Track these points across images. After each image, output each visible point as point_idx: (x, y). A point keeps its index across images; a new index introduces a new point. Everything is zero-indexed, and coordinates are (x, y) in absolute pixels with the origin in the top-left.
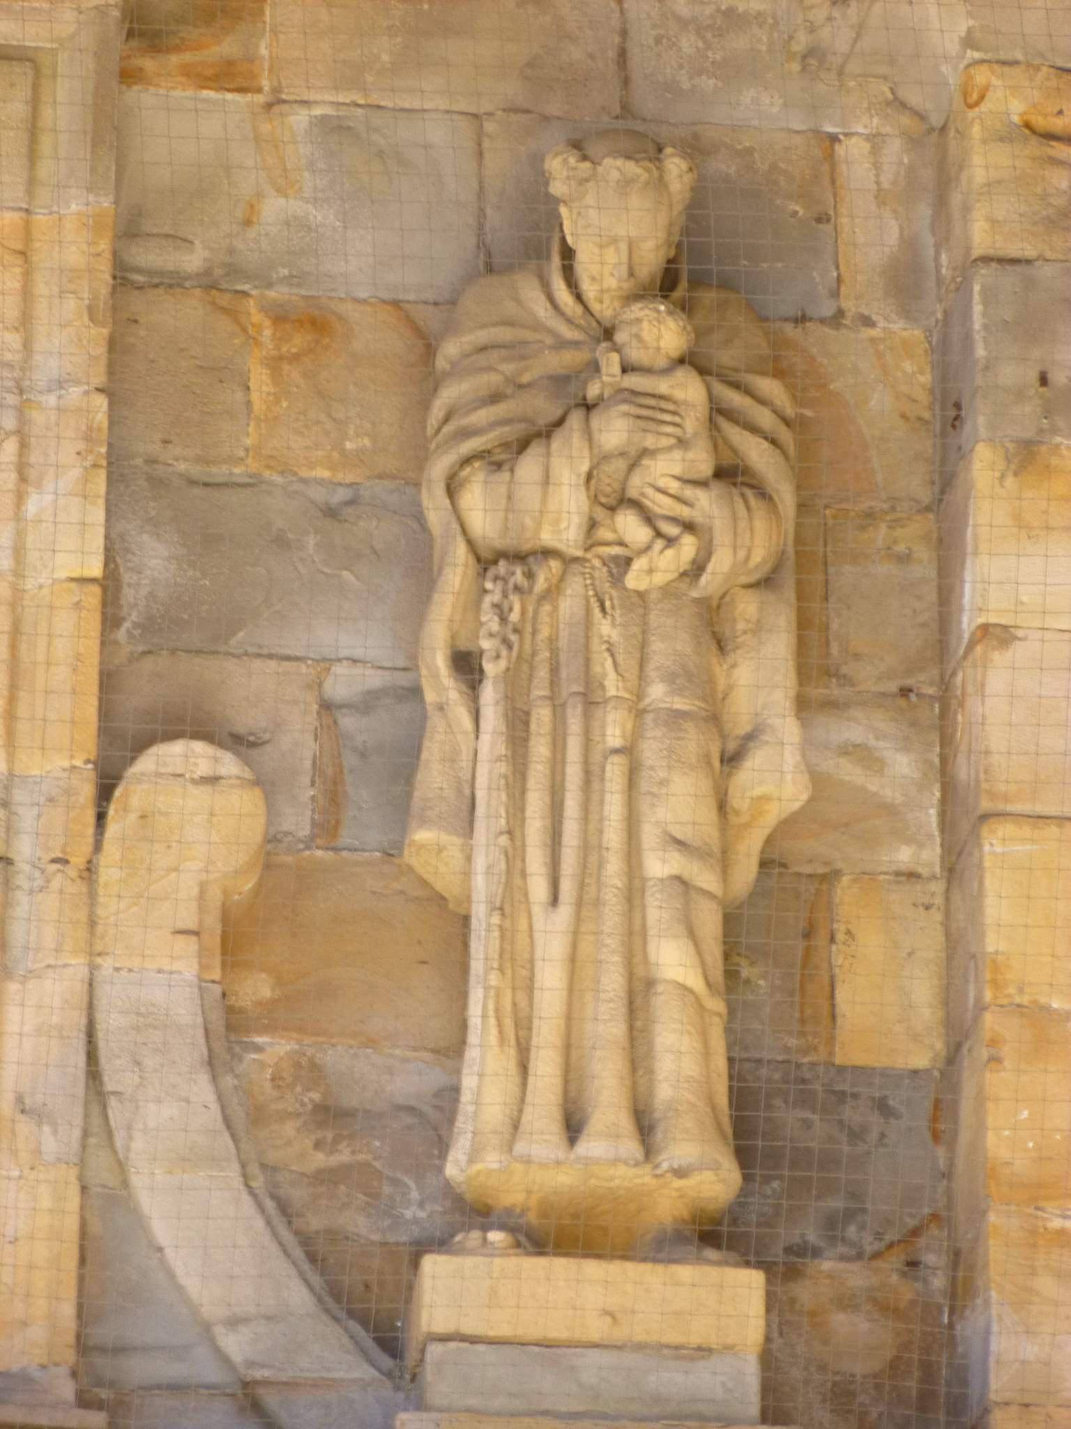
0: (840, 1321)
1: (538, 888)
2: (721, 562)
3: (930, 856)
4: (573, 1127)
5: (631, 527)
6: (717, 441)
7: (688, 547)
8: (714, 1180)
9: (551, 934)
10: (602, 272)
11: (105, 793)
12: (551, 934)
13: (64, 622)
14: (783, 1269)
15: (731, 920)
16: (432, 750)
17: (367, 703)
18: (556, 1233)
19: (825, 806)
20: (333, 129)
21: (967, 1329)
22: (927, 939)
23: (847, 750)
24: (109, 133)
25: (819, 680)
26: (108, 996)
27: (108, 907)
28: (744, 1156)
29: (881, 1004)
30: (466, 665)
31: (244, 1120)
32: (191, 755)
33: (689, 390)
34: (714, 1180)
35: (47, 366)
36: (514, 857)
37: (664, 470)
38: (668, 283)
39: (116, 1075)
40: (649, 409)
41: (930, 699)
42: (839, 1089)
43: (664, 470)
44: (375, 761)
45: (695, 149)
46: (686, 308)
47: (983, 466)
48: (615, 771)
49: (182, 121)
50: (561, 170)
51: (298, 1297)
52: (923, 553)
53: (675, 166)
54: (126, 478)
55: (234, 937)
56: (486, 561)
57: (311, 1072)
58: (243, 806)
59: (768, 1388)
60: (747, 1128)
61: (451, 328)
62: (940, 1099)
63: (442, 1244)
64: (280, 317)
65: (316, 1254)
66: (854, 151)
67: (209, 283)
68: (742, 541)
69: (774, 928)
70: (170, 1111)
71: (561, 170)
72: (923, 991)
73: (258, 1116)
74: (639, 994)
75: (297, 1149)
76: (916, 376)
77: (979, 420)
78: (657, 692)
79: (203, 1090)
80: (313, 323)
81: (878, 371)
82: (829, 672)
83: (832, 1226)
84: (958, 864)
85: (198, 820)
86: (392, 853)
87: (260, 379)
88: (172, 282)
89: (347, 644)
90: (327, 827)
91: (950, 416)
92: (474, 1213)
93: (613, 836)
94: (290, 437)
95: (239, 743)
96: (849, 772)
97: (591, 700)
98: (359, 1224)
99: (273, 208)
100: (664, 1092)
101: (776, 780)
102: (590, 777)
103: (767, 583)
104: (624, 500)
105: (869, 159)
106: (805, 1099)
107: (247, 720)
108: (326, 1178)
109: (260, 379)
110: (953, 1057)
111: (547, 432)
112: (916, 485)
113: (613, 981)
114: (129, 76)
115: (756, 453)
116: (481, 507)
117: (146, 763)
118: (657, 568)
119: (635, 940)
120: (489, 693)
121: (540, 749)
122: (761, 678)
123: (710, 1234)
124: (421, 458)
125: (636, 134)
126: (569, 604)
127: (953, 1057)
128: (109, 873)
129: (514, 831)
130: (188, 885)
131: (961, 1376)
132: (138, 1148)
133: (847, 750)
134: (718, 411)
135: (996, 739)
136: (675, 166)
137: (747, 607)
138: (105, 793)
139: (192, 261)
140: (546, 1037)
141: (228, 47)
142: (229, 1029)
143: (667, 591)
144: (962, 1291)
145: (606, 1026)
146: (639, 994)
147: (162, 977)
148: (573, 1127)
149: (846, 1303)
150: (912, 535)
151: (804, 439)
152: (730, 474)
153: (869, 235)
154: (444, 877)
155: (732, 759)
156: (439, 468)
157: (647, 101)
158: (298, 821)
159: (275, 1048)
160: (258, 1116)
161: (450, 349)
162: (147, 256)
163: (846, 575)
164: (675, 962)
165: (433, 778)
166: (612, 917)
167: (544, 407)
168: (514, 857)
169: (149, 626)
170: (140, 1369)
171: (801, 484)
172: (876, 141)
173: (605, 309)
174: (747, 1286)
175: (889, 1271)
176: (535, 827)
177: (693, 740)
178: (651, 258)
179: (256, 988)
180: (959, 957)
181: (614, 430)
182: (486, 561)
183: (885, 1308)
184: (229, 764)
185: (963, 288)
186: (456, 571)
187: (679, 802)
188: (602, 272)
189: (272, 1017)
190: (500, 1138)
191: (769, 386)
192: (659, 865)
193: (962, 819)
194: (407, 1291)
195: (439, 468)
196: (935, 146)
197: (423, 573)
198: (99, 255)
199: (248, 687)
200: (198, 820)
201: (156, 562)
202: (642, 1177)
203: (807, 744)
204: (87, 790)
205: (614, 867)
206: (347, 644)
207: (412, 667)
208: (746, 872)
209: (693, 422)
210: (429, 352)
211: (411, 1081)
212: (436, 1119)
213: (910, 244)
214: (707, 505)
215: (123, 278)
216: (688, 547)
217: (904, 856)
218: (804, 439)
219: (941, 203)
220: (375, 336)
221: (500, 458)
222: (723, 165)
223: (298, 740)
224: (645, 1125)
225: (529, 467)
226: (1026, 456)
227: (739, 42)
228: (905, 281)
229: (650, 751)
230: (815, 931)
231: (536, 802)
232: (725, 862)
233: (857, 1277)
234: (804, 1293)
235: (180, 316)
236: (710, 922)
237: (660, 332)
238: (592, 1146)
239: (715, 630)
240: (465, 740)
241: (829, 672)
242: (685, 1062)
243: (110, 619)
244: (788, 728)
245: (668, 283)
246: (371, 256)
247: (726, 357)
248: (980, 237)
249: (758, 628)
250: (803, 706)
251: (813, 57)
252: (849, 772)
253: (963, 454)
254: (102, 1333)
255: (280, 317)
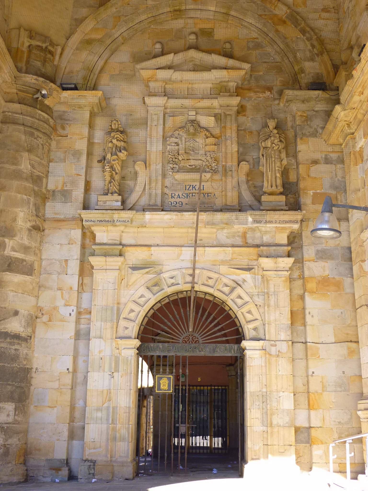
0: (291, 199)
1: (268, 170)
2: (280, 147)
3: (296, 167)
4: (272, 187)
5: (274, 145)
6: (280, 139)
7: (278, 146)
8: (282, 190)
9: (270, 174)
10: (271, 127)
11: (238, 165)
12: (270, 174)
13: (235, 154)
14: (286, 196)
15: (282, 172)
16: (261, 161)
17: (256, 158)
18: (271, 194)
19: (288, 164)
20: (252, 119)
21: (299, 199)
22: (296, 173)
23: (290, 160)
24: (236, 120)
25: (287, 155)
26: (239, 179)
27: (239, 173)
28: (283, 188)
29: (292, 177)
30: (263, 155)
31: (249, 187)
32: (245, 163)
33: (277, 135)
34: (282, 190)
35: (233, 136)
36: (267, 169)
37: (276, 141)
38: (276, 128)
39: (240, 185)
40: (275, 137)
41: (295, 156)
42: (290, 183)
43: (276, 141)
44: (257, 162)
45: (277, 119)
46: (277, 130)
47: (298, 140)
48: (273, 162)
49: (241, 119)
50: (268, 120)
51: (253, 199)
52: (294, 146)
53: (276, 120)
54: (239, 144)
55: (248, 175)
56: (264, 148)
57: (254, 184)
58: (248, 166)
59: (286, 204)
60: (283, 186)
61: (261, 132)
62: (297, 183)
63: (263, 195)
64: (249, 132)
65: (254, 196)
66: (288, 118)
67: (244, 130)
68: (282, 146)
69: (285, 172)
70: (244, 187)
71: (268, 120)
72: (295, 176)
73: (250, 187)
74: (276, 177)
75: (253, 189)
76: (293, 133)
77: (298, 136)
78: (276, 156)
79: (246, 186)
80: (251, 132)
81: (291, 134)
82: (288, 155)
83: (290, 193)
84: (297, 167)
85: (245, 167)
86: (258, 169)
87: (247, 136)
88: (241, 130)
89: (255, 154)
90: (254, 167)
91: (296, 136)
92: (265, 193)
93: (274, 166)
94: (250, 140)
95: (247, 162)
96: (290, 161)
97: (272, 157)
98: (257, 194)
99: (248, 124)
100: (278, 184)
101: (285, 162)
102: (272, 163)
103: (284, 148)
104: (273, 143)
105: (289, 119)
106: (288, 184)
107: (248, 160)
108: (255, 191)
109: (247, 136)
110: (298, 180)
111: (268, 139)
112: (294, 141)
113: (274, 177)
114: (237, 116)
115: (282, 140)
116: (263, 144)
117: (241, 163)
118: (276, 148)
119: (275, 174)
120: (264, 157)
121: (268, 161)
122: (283, 155)
123: (281, 194)
124: (259, 141)
125: (272, 117)
126: (270, 151)
127: (298, 180)
128: (239, 171)
129: (267, 167)
130: (244, 171)
131: (299, 202)
132: (242, 189)
133: (290, 160)
134: (280, 137)
135: (300, 158)
136: (276, 120)
137: (282, 150)
138: (238, 165)
139: (243, 129)
140: (269, 180)
141: (244, 113)
142: (248, 181)
143: (277, 149)
144: (299, 196)
145: (274, 180)
146: (276, 177)
147: (243, 178)
148: (272, 187)
149: (291, 198)
150: (293, 145)
151: (286, 138)
152: (281, 141)
153: (290, 124)
154: (262, 171)
155: (282, 161)
156: (260, 142)
157: (274, 116)
158: (252, 167)
159: (251, 182)
160: (250, 187)
161: (261, 133)
162: (239, 128)
163: (289, 148)
164: (278, 175)
165: (261, 163)
166: (274, 172)
167: (267, 137)
168: (267, 169)
169: (241, 154)
170: (243, 204)
171: (286, 141)
172: (290, 117)
173: (271, 130)
174: (284, 197)
175: (294, 196)
176: (268, 166)
177: (279, 160)
178: (274, 126)
179: (249, 178)
180: (298, 174)
181: (272, 138)
182: (264, 148)
183: (294, 198)
184: (247, 163)
185: (296, 127)
186: (262, 149)
187: (278, 164)
188: (271, 127)
189: (250, 180)
190: (267, 188)
191: (283, 135)
192: (277, 169)
193: (298, 164)
194: (261, 198)
195: (260, 142)
196: (294, 117)
197: (259, 149)
198: (8, 150)
199: (248, 158)
200: (245, 167)
201: (241, 149)
202: (276, 190)
203: (287, 160)
204: (237, 165)
205: (274, 169)
206: (255, 154)
207: (259, 156)
208: (283, 169)
209: (278, 137)
210: (259, 134)
211: (260, 184)
212: (262, 187)
213: (293, 124)
214: (279, 143)
215: (238, 130)
216: (278, 146)
217: (294, 167)
218: (286, 138)
219: (295, 121)
220: (255, 133)
221: (264, 141)
222: (279, 120)
223: (251, 161)
224: (276, 186)
225: (267, 141)
226: (301, 139)
227: (280, 111)
228: (292, 127)
229: (276, 161)
230: (288, 172)
231: (268, 165)
232: (281, 168)
233: (291, 196)
234: (288, 197)
235: (242, 132)
236: (280, 172)
237: (275, 131)
238: (273, 188)
239: (280, 152)
240: (263, 161)
241: (288, 155)
242: (279, 182)
243: (238, 154)
244: (285, 158)
245: (276, 128)
246: (255, 127)
247: (280, 133)
248: (297, 123)
249: (283, 152)
250: (286, 157)
251: (285, 112)
252: (290, 161)
253: (297, 139)
254: (240, 202)
255: (249, 132)
